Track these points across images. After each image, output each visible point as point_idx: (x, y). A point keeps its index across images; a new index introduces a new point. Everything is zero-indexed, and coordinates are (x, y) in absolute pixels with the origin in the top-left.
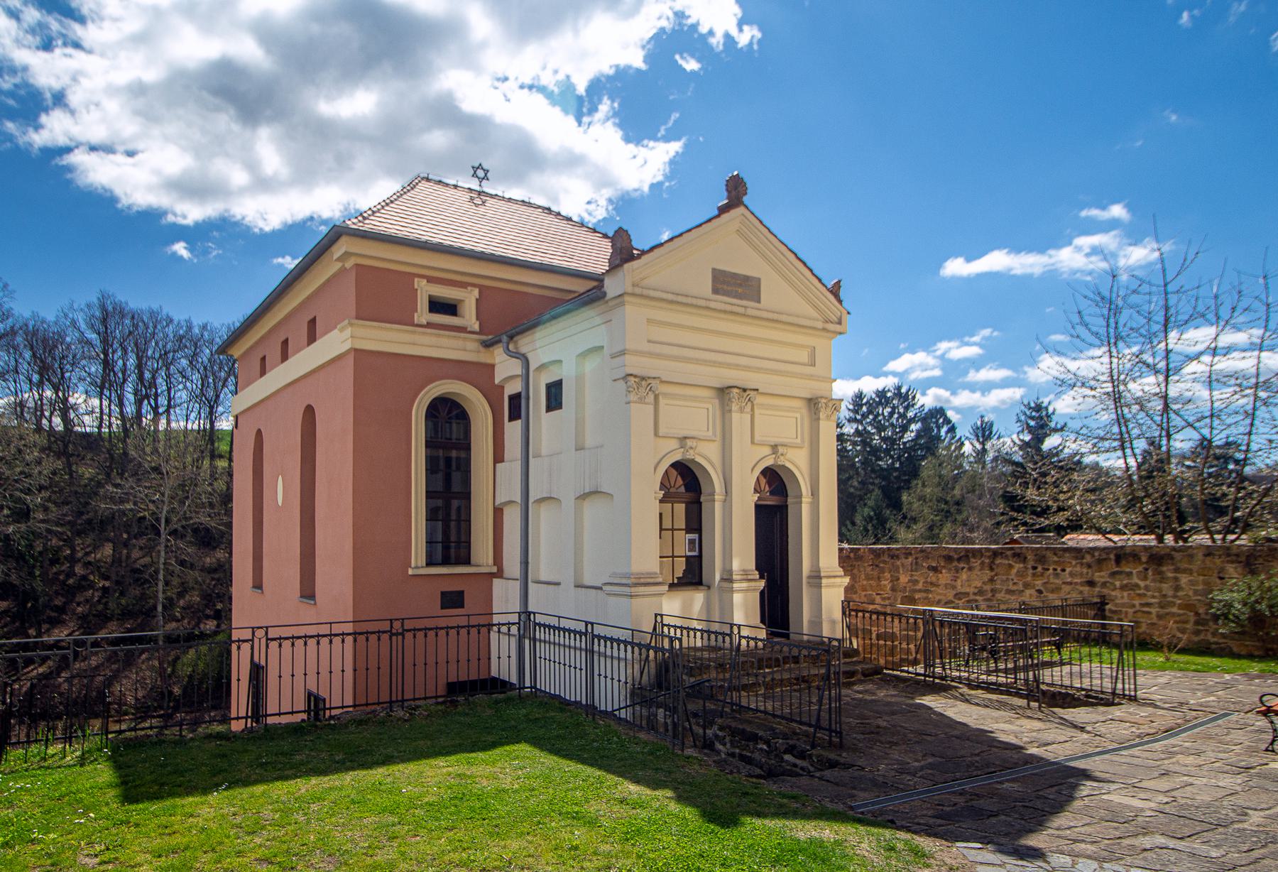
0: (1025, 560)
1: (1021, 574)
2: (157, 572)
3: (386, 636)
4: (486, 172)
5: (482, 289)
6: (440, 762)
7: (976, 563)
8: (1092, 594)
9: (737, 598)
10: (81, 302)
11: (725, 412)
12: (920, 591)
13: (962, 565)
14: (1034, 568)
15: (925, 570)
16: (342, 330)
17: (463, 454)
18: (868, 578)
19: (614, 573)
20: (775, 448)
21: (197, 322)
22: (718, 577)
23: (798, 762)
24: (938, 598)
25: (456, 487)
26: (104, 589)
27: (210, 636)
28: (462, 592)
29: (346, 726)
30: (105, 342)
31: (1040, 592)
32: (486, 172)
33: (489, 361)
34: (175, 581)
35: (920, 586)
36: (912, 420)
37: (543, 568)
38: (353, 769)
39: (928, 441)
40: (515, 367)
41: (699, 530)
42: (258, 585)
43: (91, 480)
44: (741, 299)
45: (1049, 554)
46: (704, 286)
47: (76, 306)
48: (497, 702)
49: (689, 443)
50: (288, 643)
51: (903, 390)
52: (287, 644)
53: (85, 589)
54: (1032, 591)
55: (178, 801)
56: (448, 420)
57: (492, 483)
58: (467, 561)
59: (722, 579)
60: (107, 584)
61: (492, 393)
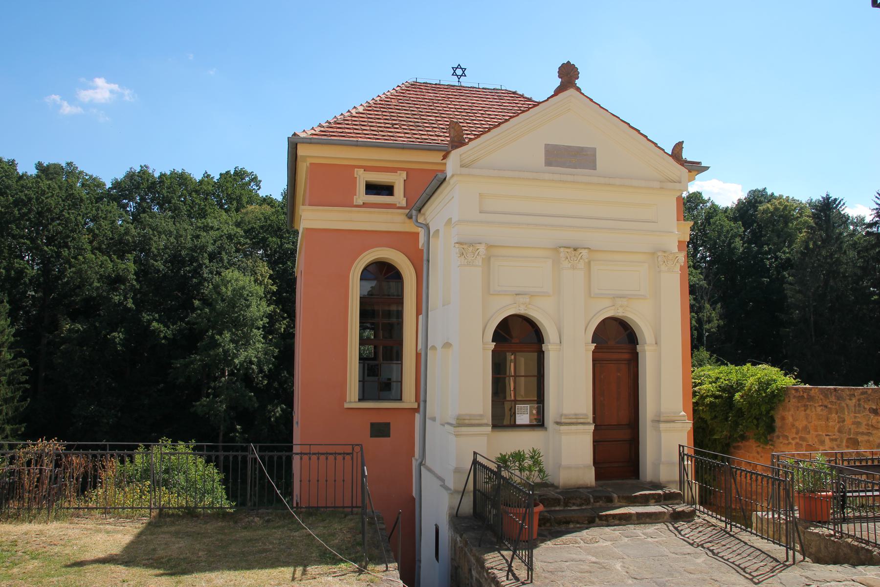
4: (464, 70)
5: (408, 171)
12: (863, 434)
15: (867, 412)
18: (819, 418)
28: (389, 424)
32: (464, 70)
35: (863, 429)
46: (540, 157)
50: (341, 457)
52: (340, 457)
58: (400, 399)
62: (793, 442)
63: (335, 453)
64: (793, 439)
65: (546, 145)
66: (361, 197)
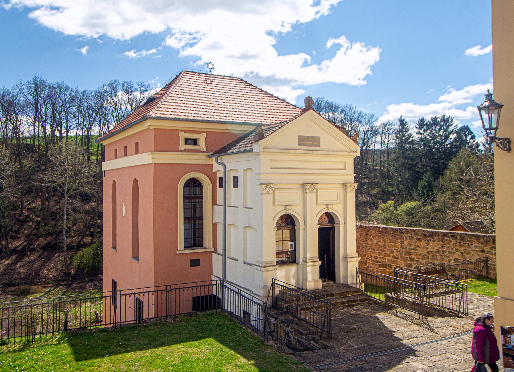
0: (456, 239)
1: (454, 245)
2: (63, 215)
3: (164, 292)
6: (181, 345)
7: (436, 238)
8: (482, 256)
9: (309, 269)
10: (24, 81)
11: (305, 193)
12: (413, 249)
13: (430, 239)
14: (460, 243)
16: (149, 154)
17: (200, 201)
18: (391, 242)
19: (257, 261)
20: (327, 205)
21: (81, 90)
22: (301, 260)
23: (315, 344)
24: (420, 253)
25: (198, 215)
26: (38, 222)
27: (88, 245)
29: (150, 325)
30: (36, 99)
31: (462, 253)
33: (210, 163)
34: (71, 218)
35: (413, 247)
36: (451, 133)
37: (232, 252)
38: (151, 348)
39: (460, 142)
40: (221, 168)
41: (294, 240)
42: (114, 247)
43: (30, 167)
44: (311, 146)
45: (466, 237)
46: (296, 145)
47: (23, 83)
48: (208, 315)
49: (288, 207)
51: (446, 117)
53: (28, 222)
54: (459, 253)
55: (95, 361)
56: (194, 184)
57: (211, 214)
59: (304, 261)
60: (39, 219)
61: (212, 176)
62: (378, 252)
63: (148, 292)
64: (377, 250)
65: (299, 136)
66: (182, 146)
